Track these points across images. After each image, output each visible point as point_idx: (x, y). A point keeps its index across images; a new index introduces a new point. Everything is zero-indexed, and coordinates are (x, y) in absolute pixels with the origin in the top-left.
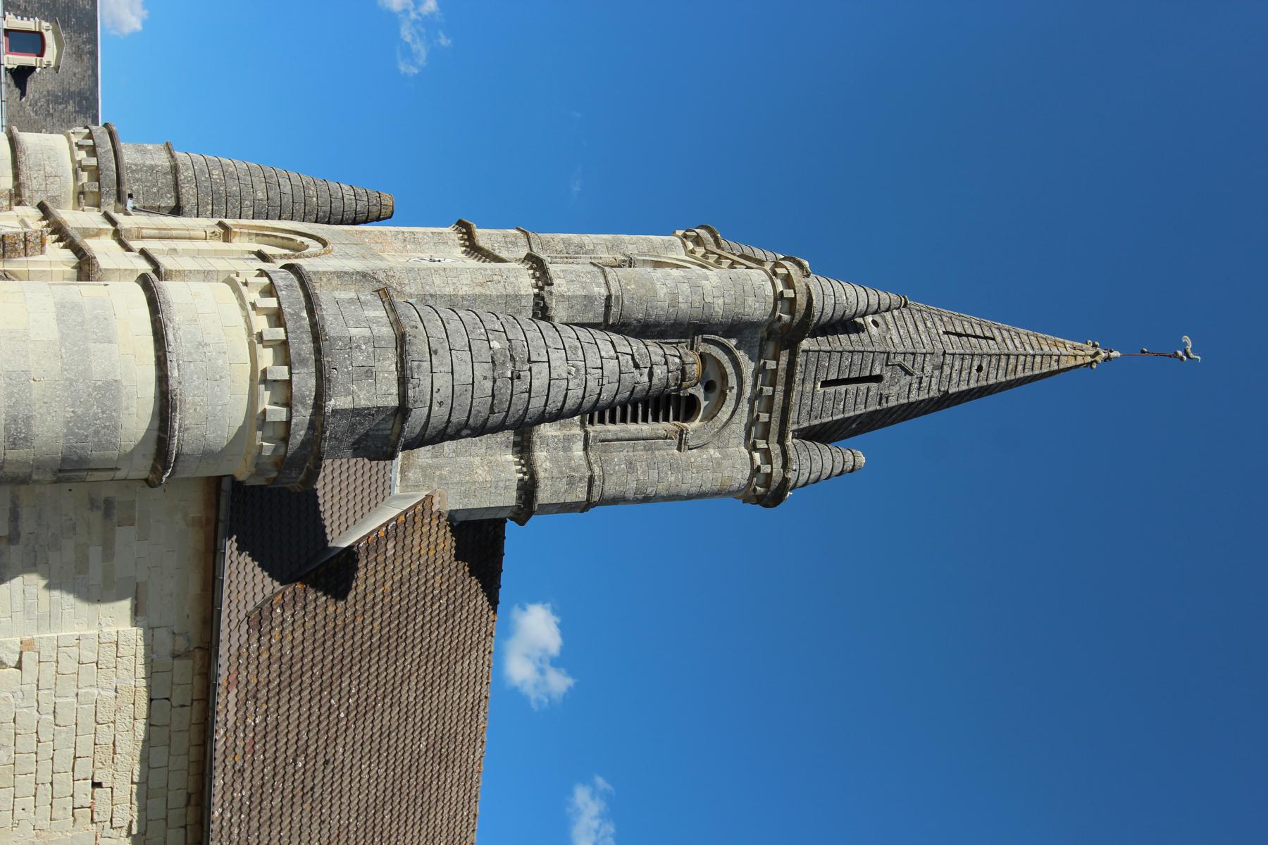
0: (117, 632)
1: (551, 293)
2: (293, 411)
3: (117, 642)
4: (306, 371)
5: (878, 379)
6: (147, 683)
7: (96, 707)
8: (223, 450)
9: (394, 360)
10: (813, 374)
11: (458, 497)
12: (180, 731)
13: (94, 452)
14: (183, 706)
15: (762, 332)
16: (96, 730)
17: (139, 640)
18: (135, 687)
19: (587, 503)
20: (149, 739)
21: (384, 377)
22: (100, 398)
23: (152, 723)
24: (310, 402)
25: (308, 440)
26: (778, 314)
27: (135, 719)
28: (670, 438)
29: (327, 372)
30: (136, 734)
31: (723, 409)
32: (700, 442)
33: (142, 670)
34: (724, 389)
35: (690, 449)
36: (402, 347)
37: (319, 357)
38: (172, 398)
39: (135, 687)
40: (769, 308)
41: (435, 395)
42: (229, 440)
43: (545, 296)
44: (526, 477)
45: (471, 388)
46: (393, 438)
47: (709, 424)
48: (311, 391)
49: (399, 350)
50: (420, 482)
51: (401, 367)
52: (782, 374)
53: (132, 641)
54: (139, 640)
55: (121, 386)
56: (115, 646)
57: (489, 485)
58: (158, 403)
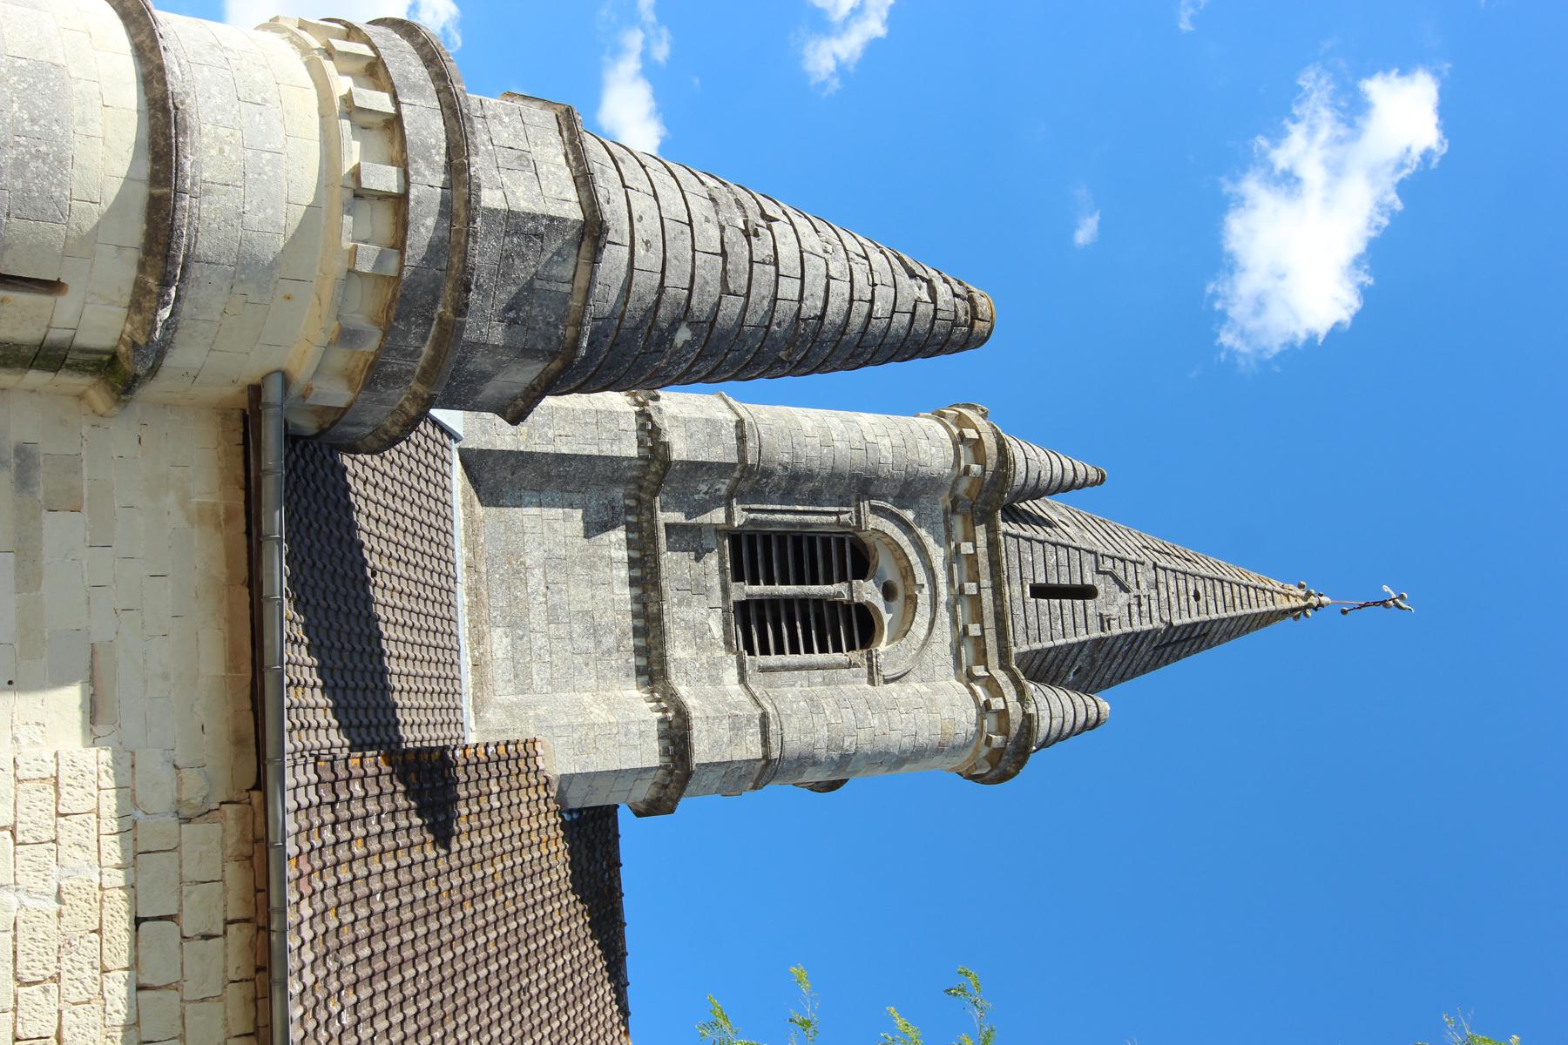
0: (56, 755)
1: (660, 410)
2: (411, 172)
3: (56, 778)
4: (424, 104)
5: (1087, 592)
6: (127, 878)
7: (15, 938)
8: (273, 265)
9: (560, 149)
10: (1018, 571)
11: (571, 752)
12: (203, 1000)
13: (13, 220)
14: (207, 937)
15: (944, 501)
16: (16, 1001)
17: (103, 775)
18: (101, 888)
19: (763, 762)
20: (137, 1024)
21: (549, 172)
22: (24, 90)
23: (144, 981)
24: (440, 159)
25: (442, 240)
26: (963, 464)
27: (105, 971)
28: (855, 665)
29: (463, 105)
30: (109, 1009)
31: (917, 618)
32: (897, 671)
33: (112, 845)
34: (910, 593)
35: (886, 682)
36: (571, 129)
37: (444, 84)
38: (176, 108)
39: (101, 888)
40: (950, 454)
41: (637, 225)
42: (289, 235)
43: (652, 413)
44: (670, 715)
45: (689, 231)
46: (575, 303)
47: (903, 642)
48: (438, 140)
49: (565, 134)
50: (506, 724)
51: (575, 159)
52: (983, 561)
53: (88, 776)
54: (103, 775)
55: (66, 77)
56: (51, 789)
57: (615, 731)
58: (146, 124)
